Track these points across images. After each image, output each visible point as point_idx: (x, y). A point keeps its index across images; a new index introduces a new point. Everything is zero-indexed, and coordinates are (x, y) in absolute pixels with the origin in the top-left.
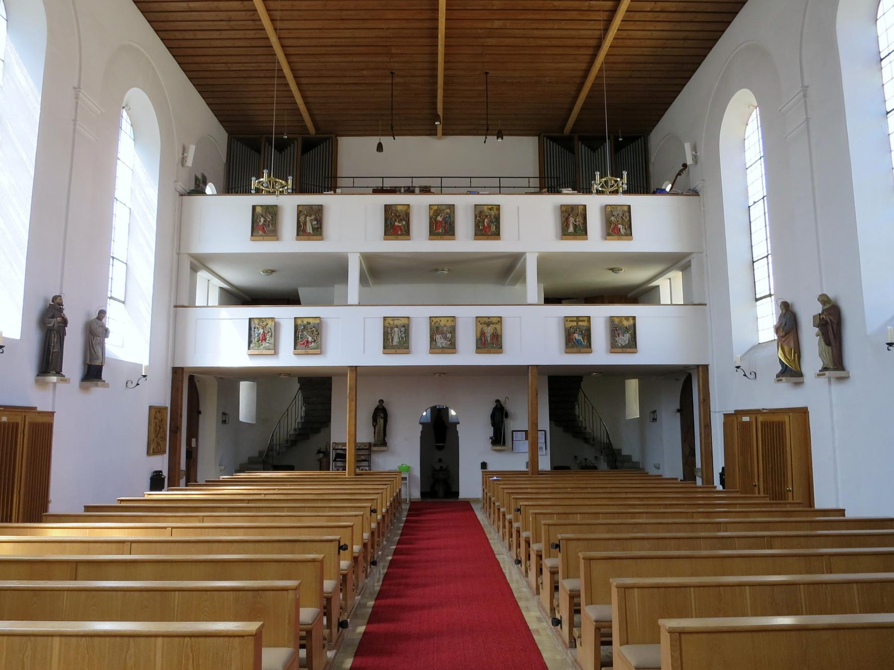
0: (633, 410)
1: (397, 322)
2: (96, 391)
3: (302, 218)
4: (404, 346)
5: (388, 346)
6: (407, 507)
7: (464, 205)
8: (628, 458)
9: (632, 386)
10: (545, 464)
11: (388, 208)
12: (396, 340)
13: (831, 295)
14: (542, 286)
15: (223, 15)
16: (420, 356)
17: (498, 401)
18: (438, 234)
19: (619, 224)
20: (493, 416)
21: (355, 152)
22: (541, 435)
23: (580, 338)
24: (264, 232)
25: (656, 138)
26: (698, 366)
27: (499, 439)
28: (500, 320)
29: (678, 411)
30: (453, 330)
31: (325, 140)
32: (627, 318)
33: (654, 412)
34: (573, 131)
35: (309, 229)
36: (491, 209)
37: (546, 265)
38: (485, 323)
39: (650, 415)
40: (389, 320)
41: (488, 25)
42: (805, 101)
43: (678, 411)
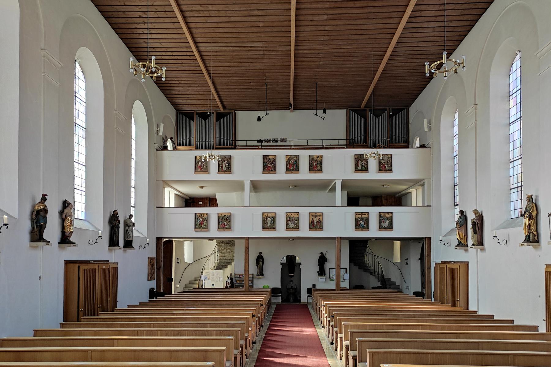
0: (397, 257)
1: (269, 215)
2: (129, 251)
3: (220, 163)
4: (273, 227)
5: (265, 227)
6: (275, 306)
7: (304, 156)
8: (394, 283)
9: (398, 244)
10: (345, 284)
11: (264, 157)
12: (269, 224)
13: (479, 211)
14: (346, 193)
15: (180, 61)
16: (281, 231)
17: (322, 253)
18: (290, 171)
19: (386, 165)
20: (319, 261)
21: (247, 123)
22: (343, 272)
23: (363, 223)
24: (201, 169)
25: (413, 109)
26: (426, 238)
27: (322, 273)
28: (322, 214)
29: (419, 259)
30: (298, 219)
31: (229, 113)
32: (388, 213)
33: (407, 259)
34: (366, 106)
35: (224, 168)
36: (318, 157)
37: (345, 185)
38: (314, 216)
39: (406, 261)
40: (265, 214)
41: (317, 63)
42: (476, 112)
43: (419, 259)
